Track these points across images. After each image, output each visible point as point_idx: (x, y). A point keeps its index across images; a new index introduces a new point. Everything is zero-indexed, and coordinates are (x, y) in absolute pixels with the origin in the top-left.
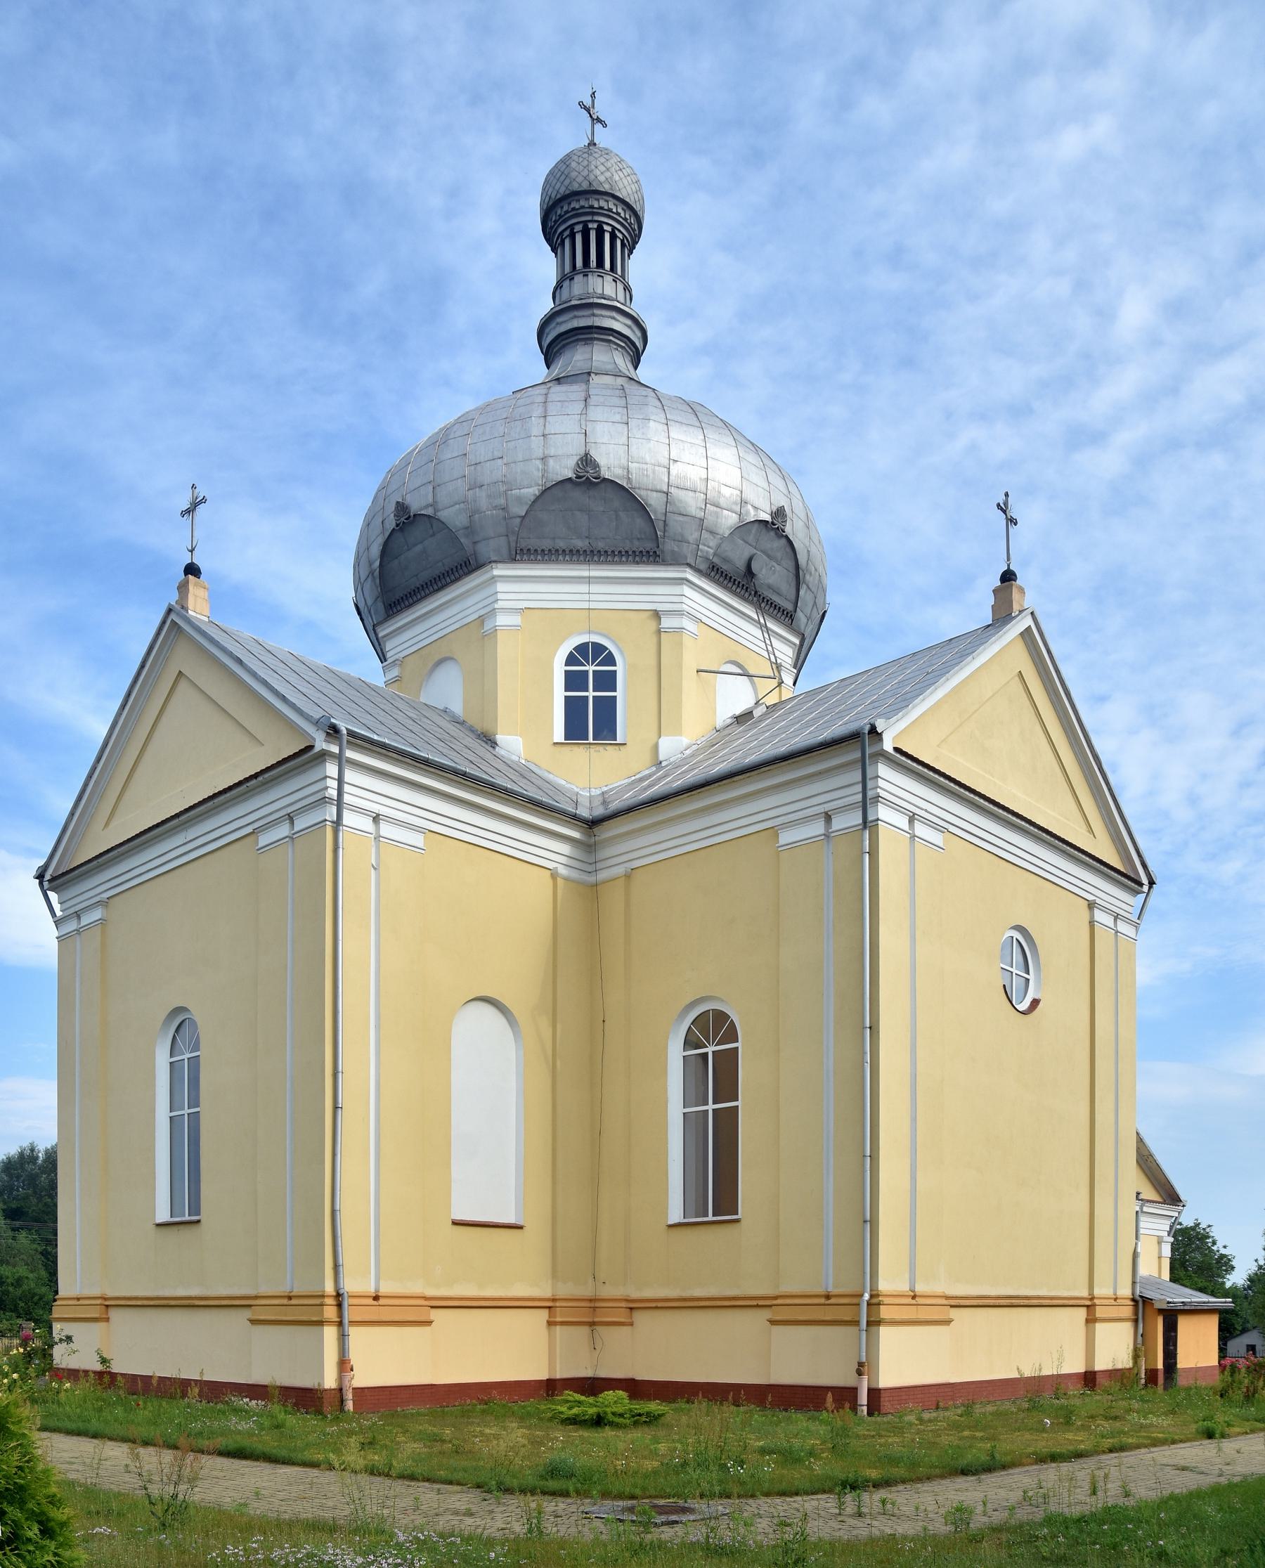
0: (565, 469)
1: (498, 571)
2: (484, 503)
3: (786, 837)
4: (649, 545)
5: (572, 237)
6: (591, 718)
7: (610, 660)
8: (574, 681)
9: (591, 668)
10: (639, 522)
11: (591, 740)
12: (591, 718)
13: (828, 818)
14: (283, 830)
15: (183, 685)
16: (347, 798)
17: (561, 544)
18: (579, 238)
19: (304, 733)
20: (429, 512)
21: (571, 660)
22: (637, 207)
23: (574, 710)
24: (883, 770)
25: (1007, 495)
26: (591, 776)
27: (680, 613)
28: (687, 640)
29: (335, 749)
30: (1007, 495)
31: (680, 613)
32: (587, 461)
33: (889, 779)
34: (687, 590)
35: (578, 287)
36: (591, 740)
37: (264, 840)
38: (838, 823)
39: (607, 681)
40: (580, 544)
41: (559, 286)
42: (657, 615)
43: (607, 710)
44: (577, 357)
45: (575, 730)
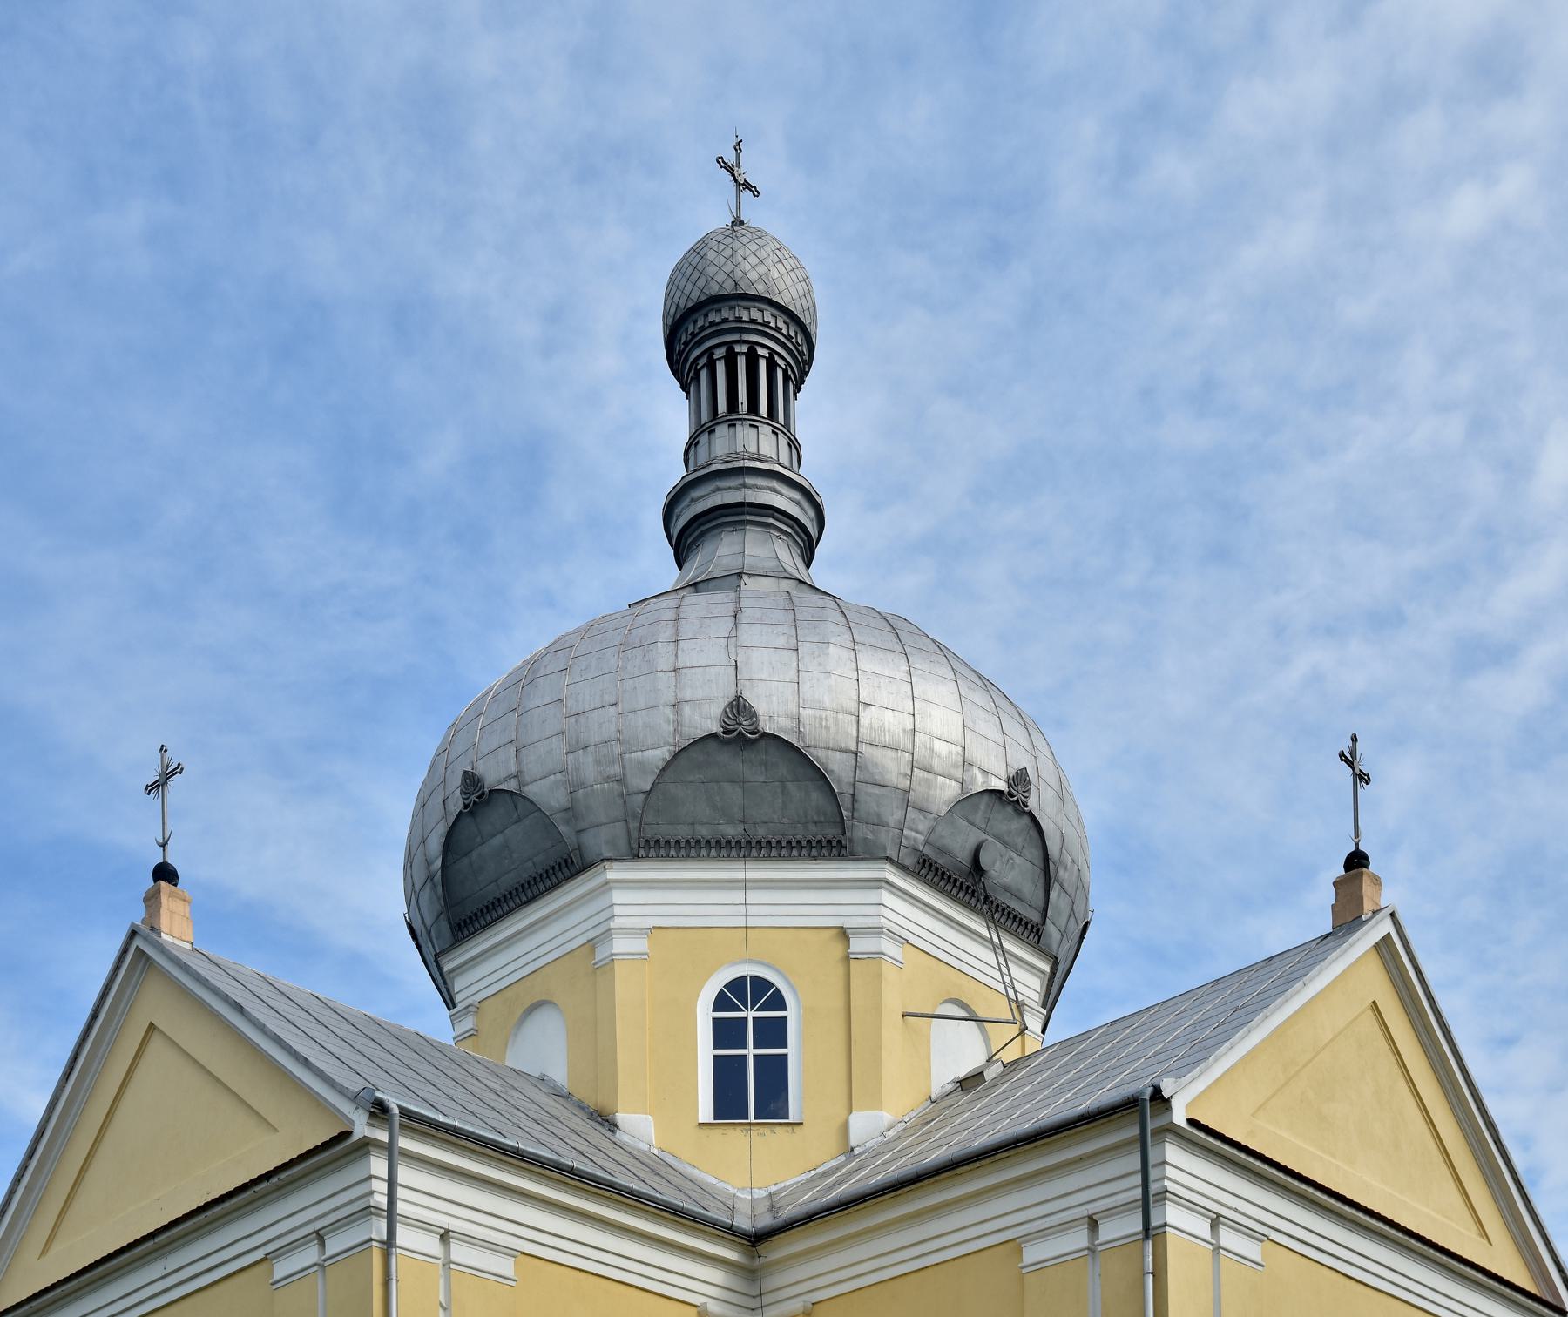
0: (707, 720)
1: (614, 872)
2: (589, 772)
3: (1032, 1254)
4: (831, 832)
5: (697, 377)
6: (751, 1085)
7: (778, 1002)
8: (726, 1033)
9: (750, 1015)
10: (816, 798)
11: (752, 1118)
12: (751, 1085)
13: (1093, 1224)
14: (310, 1255)
15: (156, 1043)
16: (401, 1207)
17: (704, 832)
18: (721, 368)
19: (336, 1113)
20: (512, 786)
21: (721, 1002)
22: (806, 320)
23: (727, 1075)
24: (1173, 1153)
25: (1354, 738)
26: (753, 1170)
27: (877, 931)
28: (887, 970)
29: (383, 1136)
30: (1354, 738)
31: (877, 931)
32: (738, 707)
33: (1181, 1166)
34: (887, 897)
35: (722, 444)
36: (752, 1118)
37: (282, 1269)
38: (1108, 1231)
39: (773, 1032)
40: (731, 831)
41: (693, 443)
42: (844, 934)
43: (774, 1074)
44: (723, 551)
45: (728, 1104)
